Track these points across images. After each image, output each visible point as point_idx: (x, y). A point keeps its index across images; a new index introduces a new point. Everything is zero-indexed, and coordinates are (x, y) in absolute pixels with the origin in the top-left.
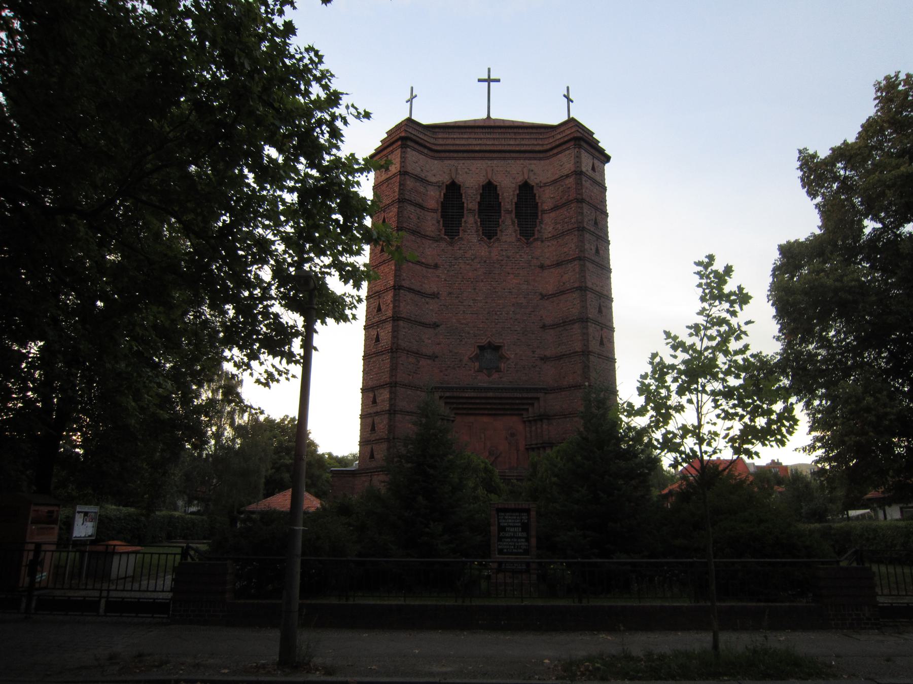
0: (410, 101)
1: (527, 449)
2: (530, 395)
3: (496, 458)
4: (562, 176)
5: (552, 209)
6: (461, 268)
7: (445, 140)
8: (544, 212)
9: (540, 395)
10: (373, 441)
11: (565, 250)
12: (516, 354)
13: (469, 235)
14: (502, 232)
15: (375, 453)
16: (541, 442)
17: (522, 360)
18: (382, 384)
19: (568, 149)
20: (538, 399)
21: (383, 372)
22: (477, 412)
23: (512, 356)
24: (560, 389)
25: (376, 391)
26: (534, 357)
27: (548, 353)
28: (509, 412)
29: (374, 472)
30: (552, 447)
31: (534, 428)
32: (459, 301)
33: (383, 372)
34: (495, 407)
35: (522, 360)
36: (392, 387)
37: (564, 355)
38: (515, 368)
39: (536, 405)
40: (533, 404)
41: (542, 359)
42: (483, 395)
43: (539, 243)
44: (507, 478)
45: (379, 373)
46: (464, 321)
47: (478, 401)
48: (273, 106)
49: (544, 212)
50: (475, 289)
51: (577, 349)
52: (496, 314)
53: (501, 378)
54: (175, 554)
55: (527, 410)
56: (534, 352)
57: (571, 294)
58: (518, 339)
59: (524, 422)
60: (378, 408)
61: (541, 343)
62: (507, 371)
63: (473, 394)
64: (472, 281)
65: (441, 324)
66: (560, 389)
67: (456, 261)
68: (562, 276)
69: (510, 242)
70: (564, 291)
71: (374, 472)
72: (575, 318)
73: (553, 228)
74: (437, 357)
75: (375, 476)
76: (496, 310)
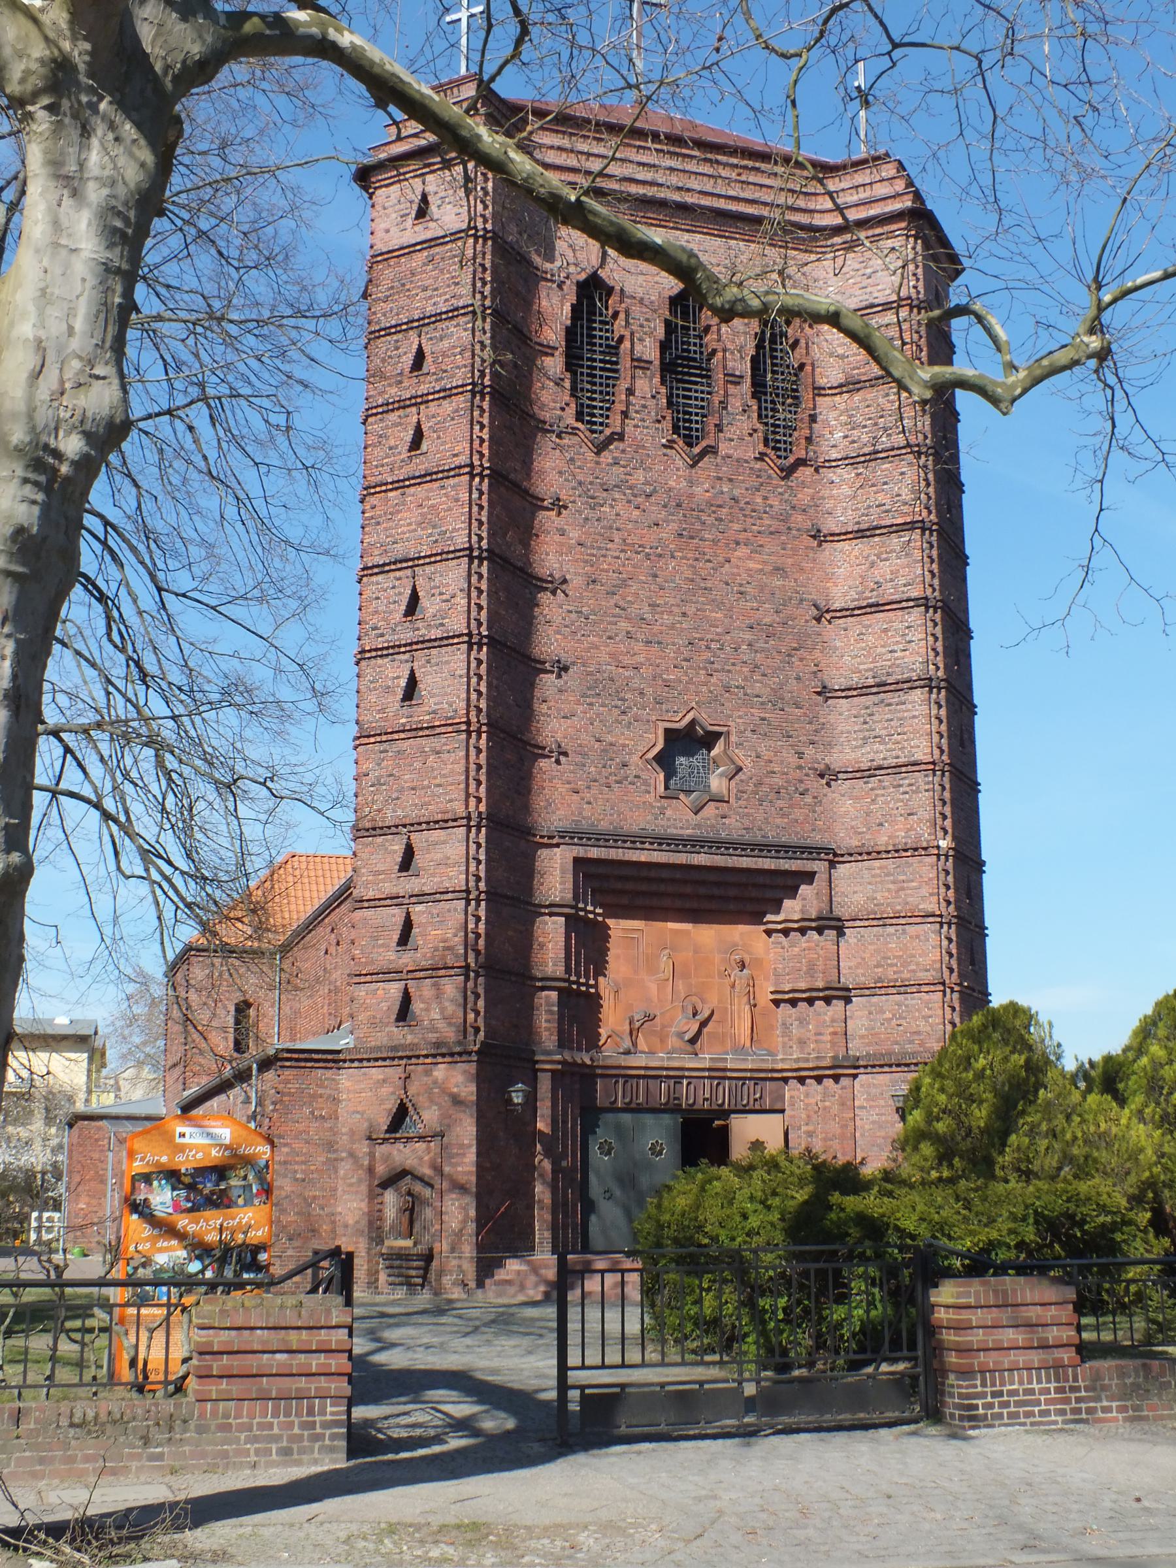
0: (848, 146)
4: (872, 306)
5: (841, 386)
6: (618, 515)
7: (564, 155)
8: (818, 391)
9: (819, 866)
11: (880, 498)
13: (636, 426)
14: (721, 431)
19: (890, 235)
28: (731, 907)
32: (616, 606)
37: (880, 768)
43: (809, 471)
44: (729, 1074)
46: (627, 661)
48: (334, 45)
49: (818, 391)
50: (655, 576)
51: (919, 756)
52: (708, 647)
54: (583, 1367)
56: (800, 755)
57: (900, 613)
58: (763, 719)
64: (648, 555)
65: (574, 663)
67: (605, 494)
68: (873, 564)
69: (738, 461)
70: (878, 605)
72: (914, 676)
73: (846, 437)
76: (709, 637)
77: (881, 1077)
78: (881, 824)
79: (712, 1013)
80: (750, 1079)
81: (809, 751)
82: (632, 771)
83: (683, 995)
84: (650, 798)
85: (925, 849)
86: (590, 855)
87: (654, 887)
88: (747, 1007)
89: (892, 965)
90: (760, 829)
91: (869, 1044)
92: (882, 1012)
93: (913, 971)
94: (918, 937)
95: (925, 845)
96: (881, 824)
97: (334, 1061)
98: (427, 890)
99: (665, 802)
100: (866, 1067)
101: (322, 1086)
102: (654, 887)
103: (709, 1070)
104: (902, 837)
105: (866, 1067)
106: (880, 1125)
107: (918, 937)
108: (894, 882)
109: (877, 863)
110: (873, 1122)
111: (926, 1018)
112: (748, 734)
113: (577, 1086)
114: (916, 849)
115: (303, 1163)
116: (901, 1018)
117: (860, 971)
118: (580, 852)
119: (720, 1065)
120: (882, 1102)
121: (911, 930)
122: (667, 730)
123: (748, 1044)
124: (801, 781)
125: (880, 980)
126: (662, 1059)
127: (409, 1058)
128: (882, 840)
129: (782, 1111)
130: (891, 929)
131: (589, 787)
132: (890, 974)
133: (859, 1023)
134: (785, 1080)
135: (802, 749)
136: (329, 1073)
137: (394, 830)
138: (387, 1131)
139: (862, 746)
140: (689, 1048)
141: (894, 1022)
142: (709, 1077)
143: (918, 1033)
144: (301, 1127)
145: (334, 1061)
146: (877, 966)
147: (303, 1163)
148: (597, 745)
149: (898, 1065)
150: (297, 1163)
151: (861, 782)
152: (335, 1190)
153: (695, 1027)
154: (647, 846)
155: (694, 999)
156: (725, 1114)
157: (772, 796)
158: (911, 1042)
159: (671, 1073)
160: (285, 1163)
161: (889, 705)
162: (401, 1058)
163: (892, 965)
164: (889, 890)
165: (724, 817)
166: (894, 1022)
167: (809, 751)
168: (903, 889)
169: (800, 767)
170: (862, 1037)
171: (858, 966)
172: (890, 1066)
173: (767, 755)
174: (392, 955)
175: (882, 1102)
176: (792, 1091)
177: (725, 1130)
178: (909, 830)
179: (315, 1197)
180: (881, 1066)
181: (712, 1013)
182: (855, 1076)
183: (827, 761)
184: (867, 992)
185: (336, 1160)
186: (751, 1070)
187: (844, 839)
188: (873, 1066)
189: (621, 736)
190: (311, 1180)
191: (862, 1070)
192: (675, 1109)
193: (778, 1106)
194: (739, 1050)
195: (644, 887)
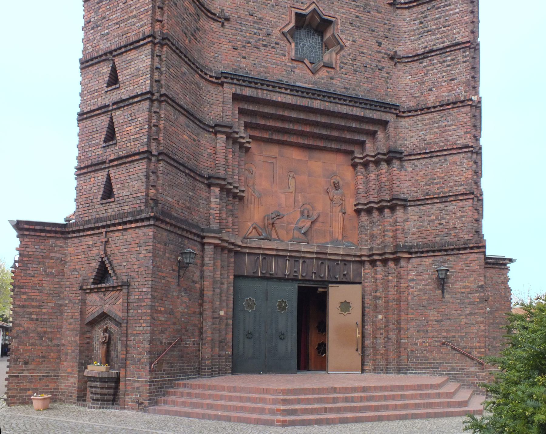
1: (358, 212)
2: (376, 115)
3: (313, 223)
9: (389, 117)
10: (111, 161)
12: (354, 41)
15: (116, 187)
16: (388, 198)
17: (363, 53)
18: (133, 39)
20: (384, 124)
21: (135, 17)
22: (286, 138)
23: (348, 44)
24: (426, 110)
25: (116, 60)
26: (379, 52)
27: (401, 50)
29: (114, 225)
30: (405, 207)
31: (372, 176)
33: (135, 17)
34: (316, 131)
35: (363, 53)
36: (155, 44)
37: (432, 51)
38: (353, 65)
39: (380, 135)
40: (373, 134)
41: (392, 58)
42: (305, 102)
44: (329, 257)
45: (123, 21)
47: (294, 115)
51: (459, 39)
53: (332, 79)
55: (362, 144)
56: (380, 44)
58: (357, 17)
59: (354, 166)
60: (123, 93)
61: (389, 29)
62: (341, 68)
63: (288, 99)
66: (426, 110)
71: (114, 225)
74: (227, 19)
75: (117, 234)
77: (427, 260)
78: (431, 89)
79: (319, 216)
80: (342, 260)
81: (385, 43)
82: (273, 39)
83: (301, 204)
84: (286, 59)
85: (462, 102)
86: (244, 93)
87: (286, 126)
88: (341, 214)
89: (436, 183)
90: (354, 90)
91: (418, 238)
92: (429, 215)
93: (452, 187)
94: (455, 163)
95: (462, 98)
96: (431, 89)
97: (62, 233)
98: (124, 97)
99: (295, 64)
100: (416, 253)
101: (52, 251)
102: (286, 126)
103: (317, 253)
104: (445, 95)
105: (416, 253)
106: (425, 292)
107: (455, 163)
108: (439, 127)
109: (427, 116)
110: (421, 290)
111: (460, 218)
112: (348, 25)
113: (232, 260)
114: (455, 103)
115: (38, 307)
116: (442, 219)
117: (413, 189)
118: (238, 90)
119: (323, 251)
120: (427, 276)
121: (451, 159)
122: (297, 14)
123: (340, 238)
124: (380, 62)
125: (428, 194)
126: (288, 244)
127: (109, 226)
128: (431, 100)
129: (360, 283)
130: (436, 160)
131: (244, 47)
132: (435, 189)
133: (412, 224)
134: (362, 263)
135: (381, 40)
136: (58, 242)
137: (104, 57)
138: (93, 283)
139: (419, 39)
140: (303, 237)
141: (437, 222)
142: (316, 258)
143: (454, 228)
144: (36, 280)
145: (62, 233)
146: (427, 185)
147: (38, 307)
148: (251, 18)
149: (440, 251)
150: (33, 307)
151: (417, 63)
152: (61, 327)
153: (308, 224)
154: (283, 91)
155: (308, 207)
156: (325, 284)
157: (362, 69)
158: (449, 235)
159: (293, 254)
160: (23, 306)
161: (439, 8)
162: (103, 227)
163: (436, 183)
164: (435, 133)
165: (332, 79)
166: (437, 222)
167: (385, 43)
168: (445, 131)
169: (379, 52)
170: (414, 233)
171: (413, 186)
172: (433, 251)
173: (360, 41)
174: (100, 151)
175: (427, 276)
176: (367, 270)
177: (324, 297)
178: (450, 91)
179: (45, 332)
180: (428, 252)
181: (319, 216)
182: (409, 259)
183: (396, 49)
184: (419, 203)
185: (61, 305)
186: (342, 255)
187: (406, 102)
188: (422, 252)
189: (269, 15)
190: (43, 320)
191: (414, 255)
192: (295, 280)
193: (357, 280)
194: (334, 241)
195: (279, 125)
